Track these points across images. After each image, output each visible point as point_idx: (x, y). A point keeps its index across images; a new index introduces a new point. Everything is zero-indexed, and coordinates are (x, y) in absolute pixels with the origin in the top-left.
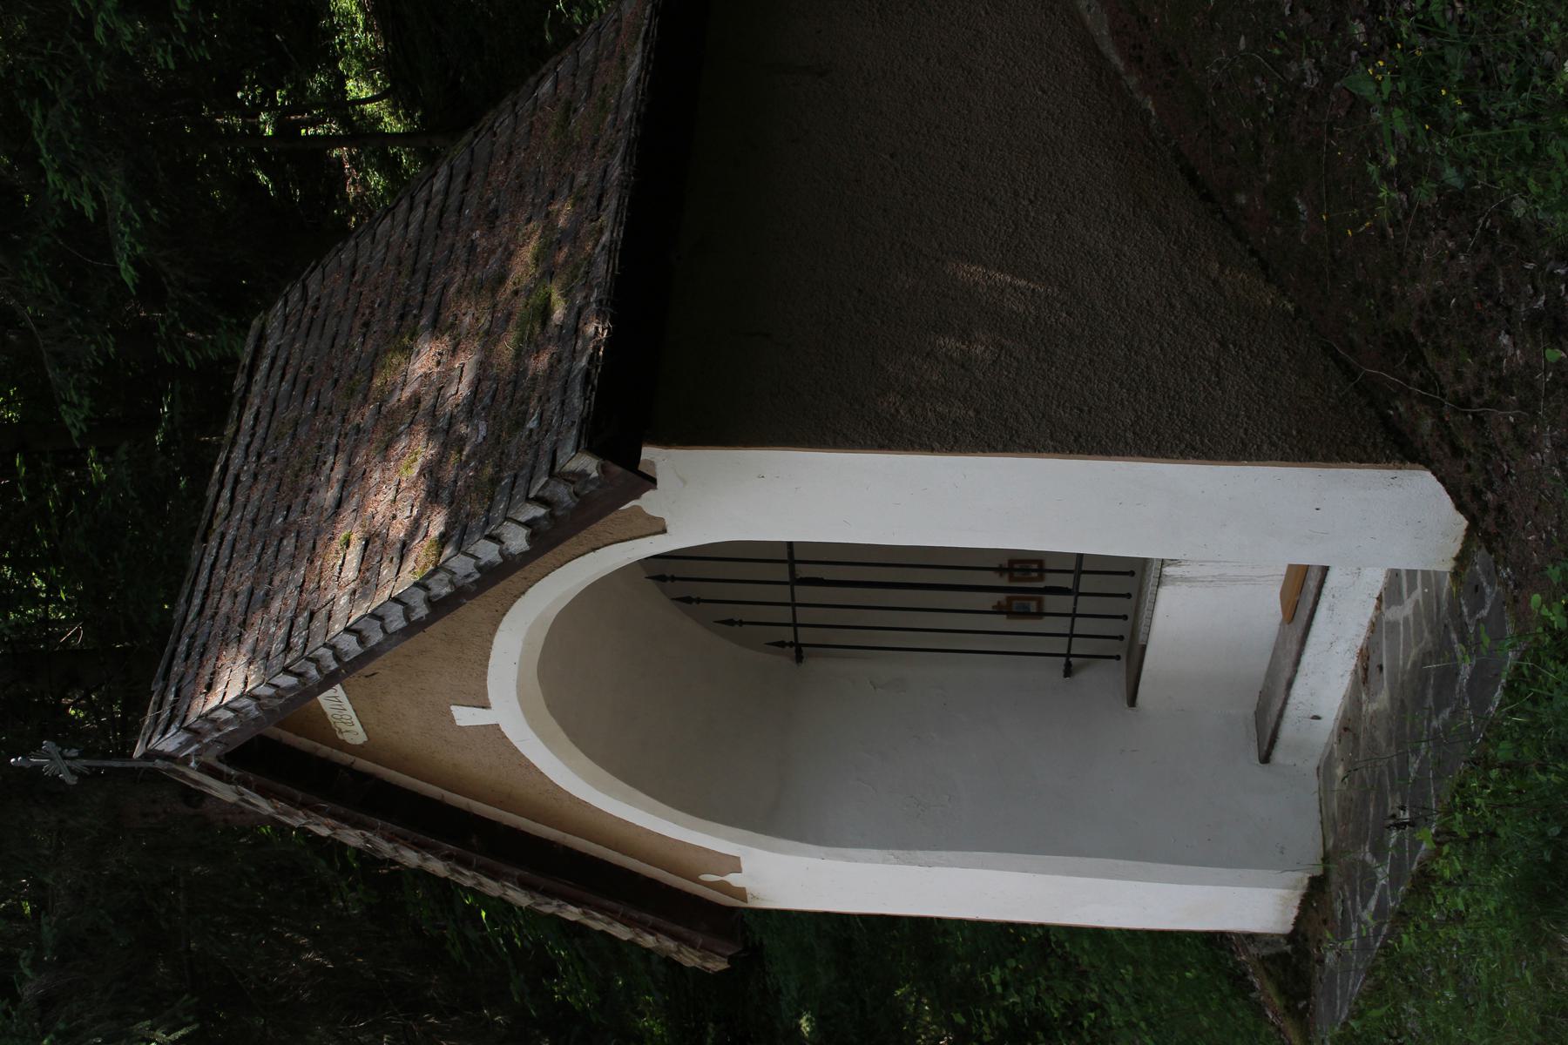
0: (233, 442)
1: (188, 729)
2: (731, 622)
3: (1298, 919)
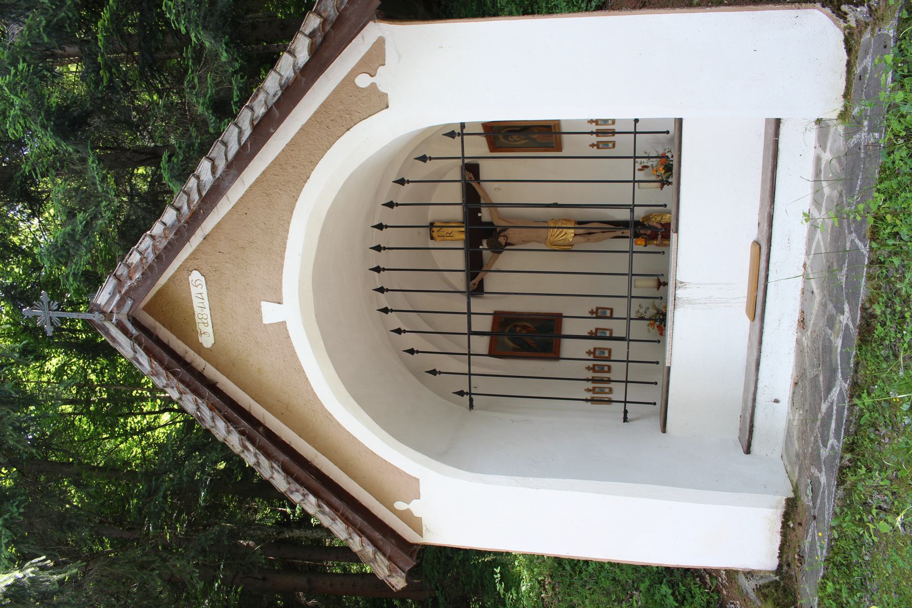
2: (434, 372)
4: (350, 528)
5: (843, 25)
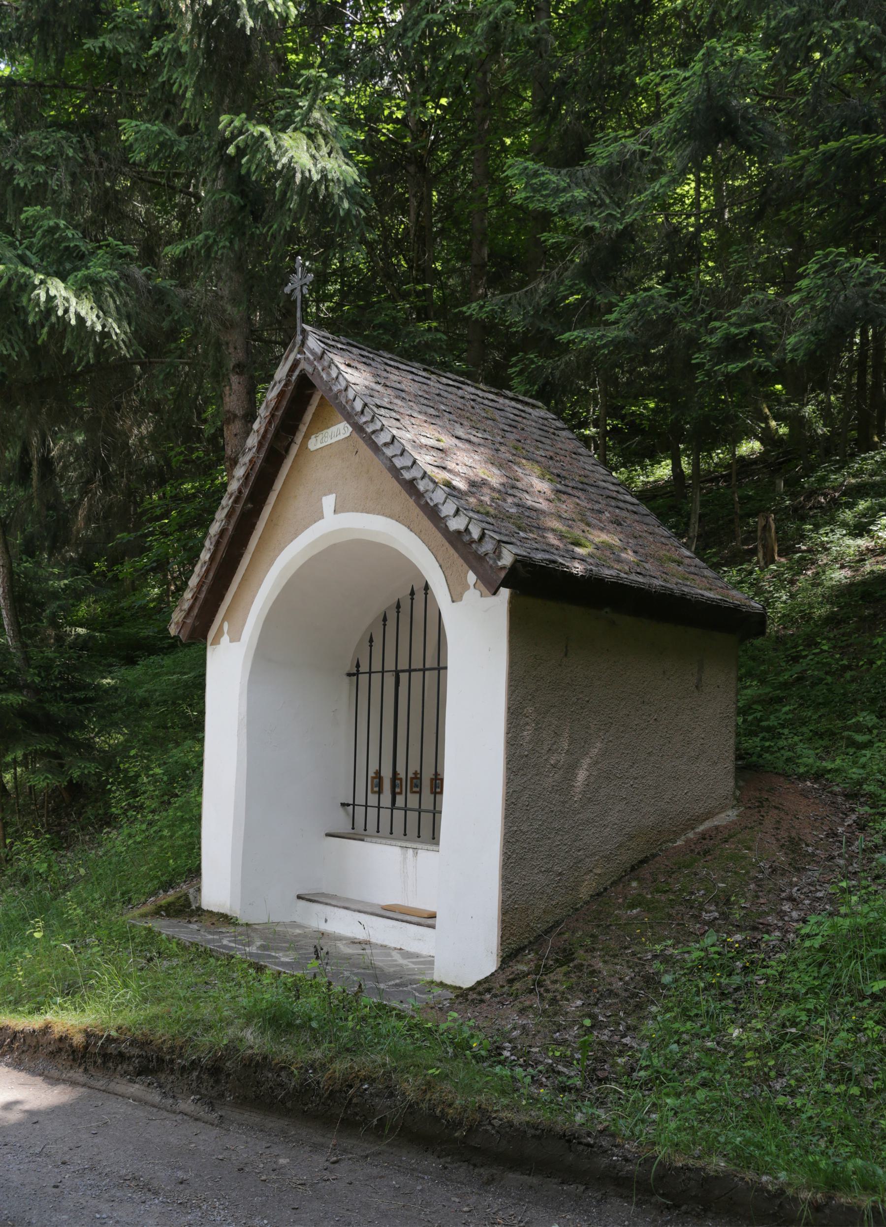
0: (477, 388)
1: (323, 353)
2: (371, 641)
3: (211, 912)
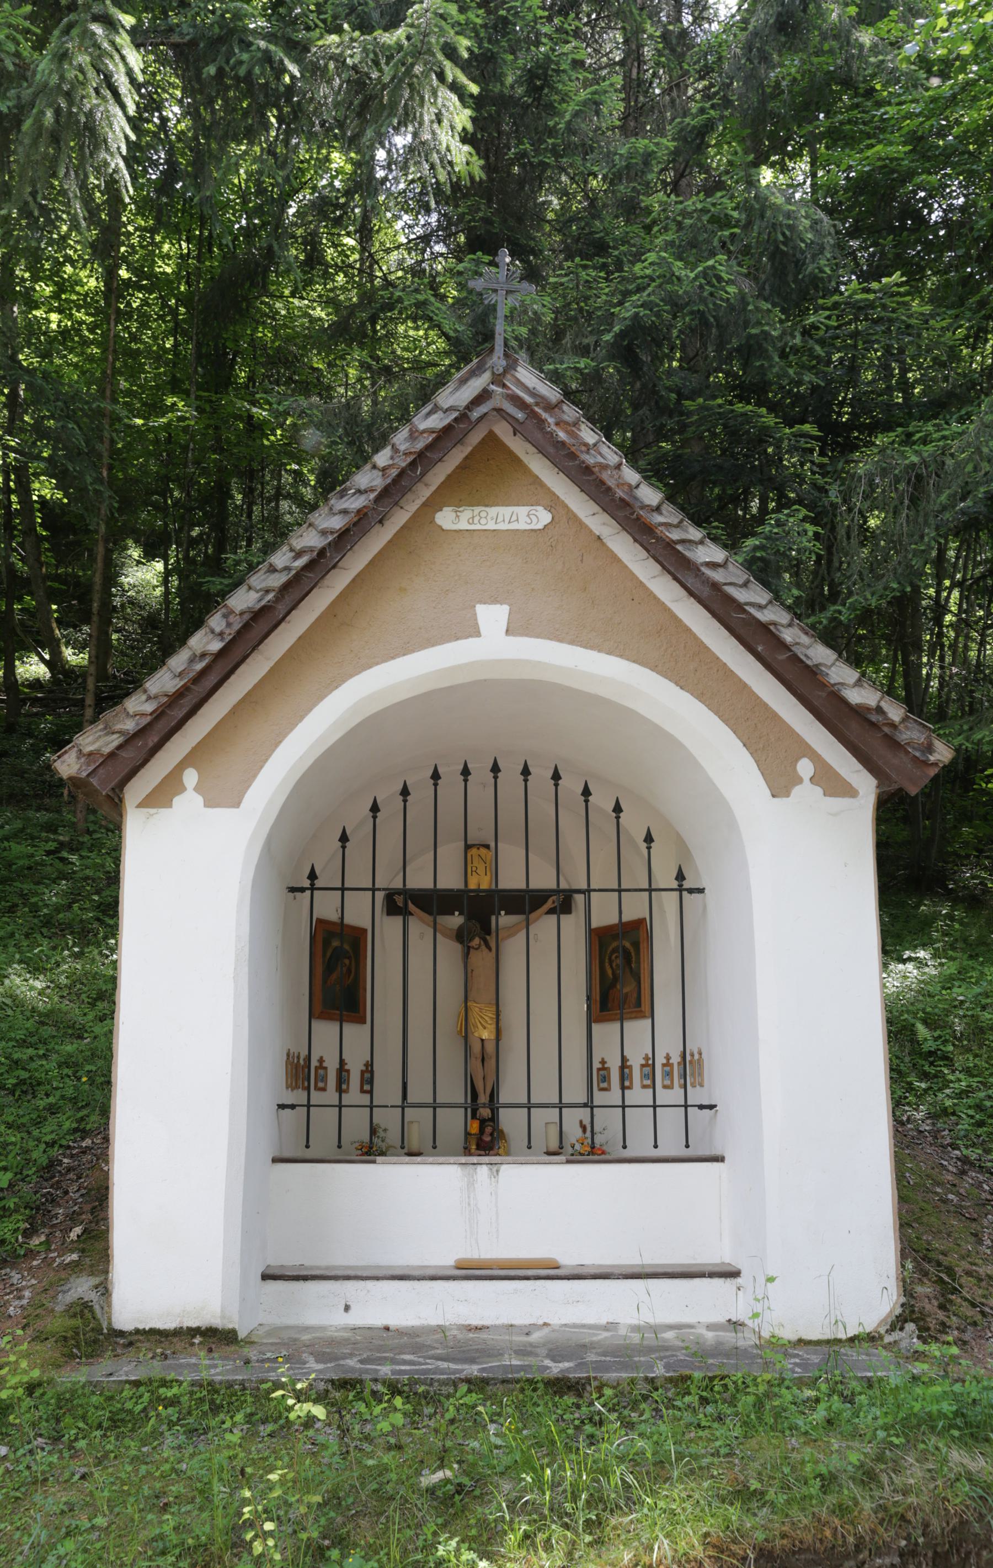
4: (166, 699)
5: (882, 1330)
